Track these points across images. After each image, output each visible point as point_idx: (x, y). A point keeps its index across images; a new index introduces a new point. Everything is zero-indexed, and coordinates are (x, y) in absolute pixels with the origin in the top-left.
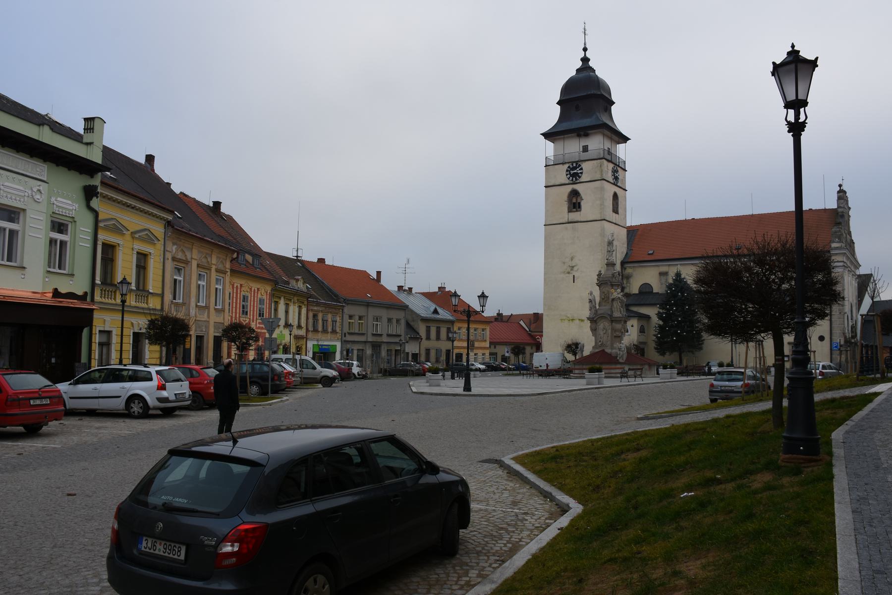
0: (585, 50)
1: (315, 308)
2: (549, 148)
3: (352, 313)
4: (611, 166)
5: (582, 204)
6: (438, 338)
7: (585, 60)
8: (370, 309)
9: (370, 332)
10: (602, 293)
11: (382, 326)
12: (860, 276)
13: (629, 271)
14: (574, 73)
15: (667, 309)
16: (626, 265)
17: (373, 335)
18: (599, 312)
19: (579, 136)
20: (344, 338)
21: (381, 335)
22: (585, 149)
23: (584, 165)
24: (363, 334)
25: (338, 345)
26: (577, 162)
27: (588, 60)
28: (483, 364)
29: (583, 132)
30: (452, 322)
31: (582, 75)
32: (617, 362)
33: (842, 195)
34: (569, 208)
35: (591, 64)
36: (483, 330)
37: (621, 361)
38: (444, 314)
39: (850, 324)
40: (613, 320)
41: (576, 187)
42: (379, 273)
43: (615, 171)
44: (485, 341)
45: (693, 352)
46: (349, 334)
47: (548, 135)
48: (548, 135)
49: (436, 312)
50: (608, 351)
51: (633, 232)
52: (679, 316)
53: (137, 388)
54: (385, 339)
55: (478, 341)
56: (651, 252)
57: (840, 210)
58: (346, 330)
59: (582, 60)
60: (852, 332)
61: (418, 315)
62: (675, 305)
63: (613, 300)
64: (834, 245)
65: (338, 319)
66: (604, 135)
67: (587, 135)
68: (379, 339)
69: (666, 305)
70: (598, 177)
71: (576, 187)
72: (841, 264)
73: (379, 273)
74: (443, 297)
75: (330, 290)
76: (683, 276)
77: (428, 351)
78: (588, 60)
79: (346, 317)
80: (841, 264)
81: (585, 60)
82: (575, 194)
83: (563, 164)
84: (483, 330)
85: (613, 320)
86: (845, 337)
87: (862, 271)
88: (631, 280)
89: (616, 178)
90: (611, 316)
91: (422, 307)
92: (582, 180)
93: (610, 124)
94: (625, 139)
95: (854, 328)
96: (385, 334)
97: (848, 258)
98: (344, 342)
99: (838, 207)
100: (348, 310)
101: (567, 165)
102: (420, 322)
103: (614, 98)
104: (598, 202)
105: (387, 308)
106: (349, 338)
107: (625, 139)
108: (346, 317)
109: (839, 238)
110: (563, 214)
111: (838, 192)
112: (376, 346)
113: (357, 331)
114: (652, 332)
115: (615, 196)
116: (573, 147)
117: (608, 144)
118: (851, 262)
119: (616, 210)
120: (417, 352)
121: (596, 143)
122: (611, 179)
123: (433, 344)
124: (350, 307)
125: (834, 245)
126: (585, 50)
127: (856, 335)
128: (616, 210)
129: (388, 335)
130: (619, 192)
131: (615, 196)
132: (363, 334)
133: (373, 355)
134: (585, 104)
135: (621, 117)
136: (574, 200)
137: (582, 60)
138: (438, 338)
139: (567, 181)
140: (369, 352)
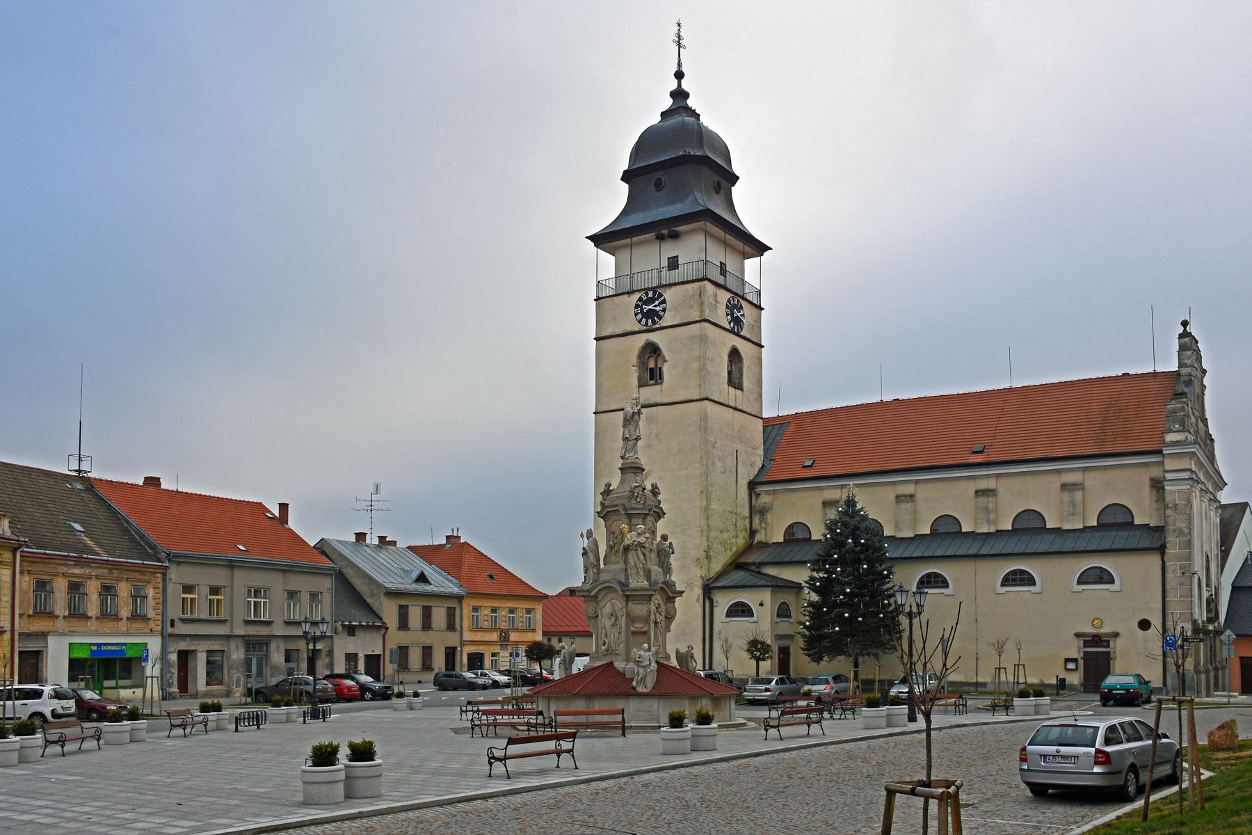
0: (679, 75)
1: (77, 571)
2: (607, 263)
3: (190, 581)
4: (724, 296)
5: (665, 369)
6: (427, 625)
7: (679, 95)
8: (239, 574)
9: (239, 615)
10: (610, 533)
11: (286, 606)
12: (1224, 507)
13: (765, 499)
14: (656, 119)
15: (827, 571)
16: (760, 489)
17: (248, 623)
18: (603, 577)
19: (661, 238)
20: (170, 630)
21: (269, 623)
22: (673, 263)
23: (668, 294)
24: (224, 621)
25: (154, 645)
26: (654, 289)
27: (686, 95)
28: (507, 673)
29: (666, 230)
30: (459, 598)
31: (671, 122)
32: (632, 694)
33: (1188, 343)
34: (640, 379)
35: (690, 102)
36: (528, 611)
37: (640, 689)
38: (440, 582)
39: (1205, 594)
40: (630, 597)
41: (653, 337)
42: (284, 507)
43: (732, 308)
44: (534, 630)
45: (877, 657)
46: (184, 621)
47: (599, 240)
48: (599, 240)
49: (422, 578)
50: (619, 665)
51: (773, 427)
52: (848, 584)
53: (34, 705)
54: (279, 630)
55: (517, 630)
56: (808, 463)
57: (1184, 371)
58: (174, 611)
59: (673, 94)
60: (1209, 611)
61: (379, 585)
62: (842, 561)
63: (627, 549)
64: (1170, 438)
65: (151, 592)
66: (706, 233)
67: (675, 236)
68: (263, 631)
69: (825, 562)
70: (696, 315)
71: (653, 337)
72: (1186, 475)
73: (284, 507)
74: (452, 554)
75: (142, 536)
76: (859, 506)
77: (403, 651)
78: (686, 95)
79: (175, 591)
80: (1186, 475)
81: (679, 95)
82: (652, 350)
83: (629, 293)
84: (528, 611)
85: (630, 597)
86: (1194, 622)
87: (1225, 497)
88: (769, 516)
89: (737, 321)
90: (624, 585)
91: (392, 572)
92: (664, 323)
93: (726, 216)
94: (760, 248)
95: (1212, 603)
96: (278, 620)
97: (1199, 462)
98: (166, 638)
99: (1180, 366)
100: (176, 574)
101: (636, 296)
102: (384, 599)
103: (736, 168)
104: (695, 365)
105: (284, 571)
106: (181, 629)
107: (760, 248)
108: (175, 591)
109: (1182, 424)
110: (630, 390)
111: (1181, 336)
112: (256, 645)
113: (205, 615)
114: (801, 617)
115: (735, 354)
116: (650, 260)
117: (716, 255)
118: (1207, 473)
119: (735, 381)
120: (378, 651)
121: (694, 250)
122: (725, 322)
123: (415, 637)
124: (183, 568)
125: (1170, 438)
126: (679, 75)
127: (1217, 617)
128: (735, 381)
129: (288, 623)
130: (744, 348)
131: (735, 354)
132: (224, 621)
133: (248, 662)
134: (679, 174)
135: (750, 205)
136: (652, 364)
137: (673, 94)
138: (427, 625)
139: (637, 327)
140: (237, 654)
